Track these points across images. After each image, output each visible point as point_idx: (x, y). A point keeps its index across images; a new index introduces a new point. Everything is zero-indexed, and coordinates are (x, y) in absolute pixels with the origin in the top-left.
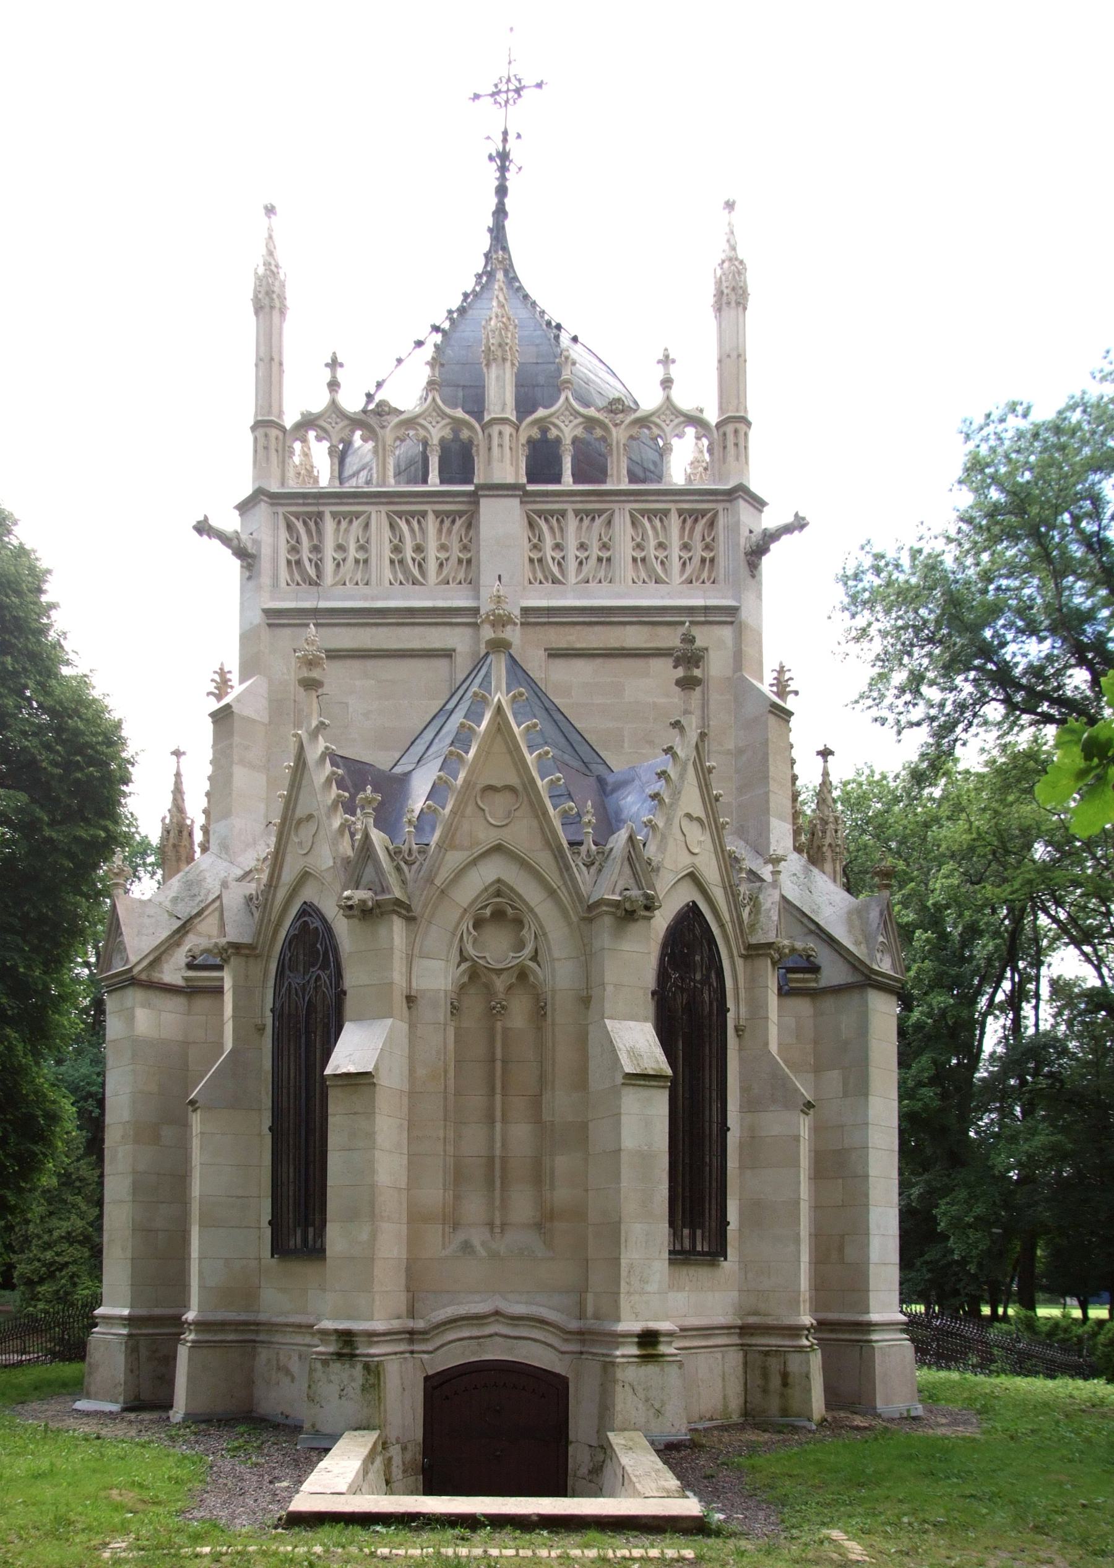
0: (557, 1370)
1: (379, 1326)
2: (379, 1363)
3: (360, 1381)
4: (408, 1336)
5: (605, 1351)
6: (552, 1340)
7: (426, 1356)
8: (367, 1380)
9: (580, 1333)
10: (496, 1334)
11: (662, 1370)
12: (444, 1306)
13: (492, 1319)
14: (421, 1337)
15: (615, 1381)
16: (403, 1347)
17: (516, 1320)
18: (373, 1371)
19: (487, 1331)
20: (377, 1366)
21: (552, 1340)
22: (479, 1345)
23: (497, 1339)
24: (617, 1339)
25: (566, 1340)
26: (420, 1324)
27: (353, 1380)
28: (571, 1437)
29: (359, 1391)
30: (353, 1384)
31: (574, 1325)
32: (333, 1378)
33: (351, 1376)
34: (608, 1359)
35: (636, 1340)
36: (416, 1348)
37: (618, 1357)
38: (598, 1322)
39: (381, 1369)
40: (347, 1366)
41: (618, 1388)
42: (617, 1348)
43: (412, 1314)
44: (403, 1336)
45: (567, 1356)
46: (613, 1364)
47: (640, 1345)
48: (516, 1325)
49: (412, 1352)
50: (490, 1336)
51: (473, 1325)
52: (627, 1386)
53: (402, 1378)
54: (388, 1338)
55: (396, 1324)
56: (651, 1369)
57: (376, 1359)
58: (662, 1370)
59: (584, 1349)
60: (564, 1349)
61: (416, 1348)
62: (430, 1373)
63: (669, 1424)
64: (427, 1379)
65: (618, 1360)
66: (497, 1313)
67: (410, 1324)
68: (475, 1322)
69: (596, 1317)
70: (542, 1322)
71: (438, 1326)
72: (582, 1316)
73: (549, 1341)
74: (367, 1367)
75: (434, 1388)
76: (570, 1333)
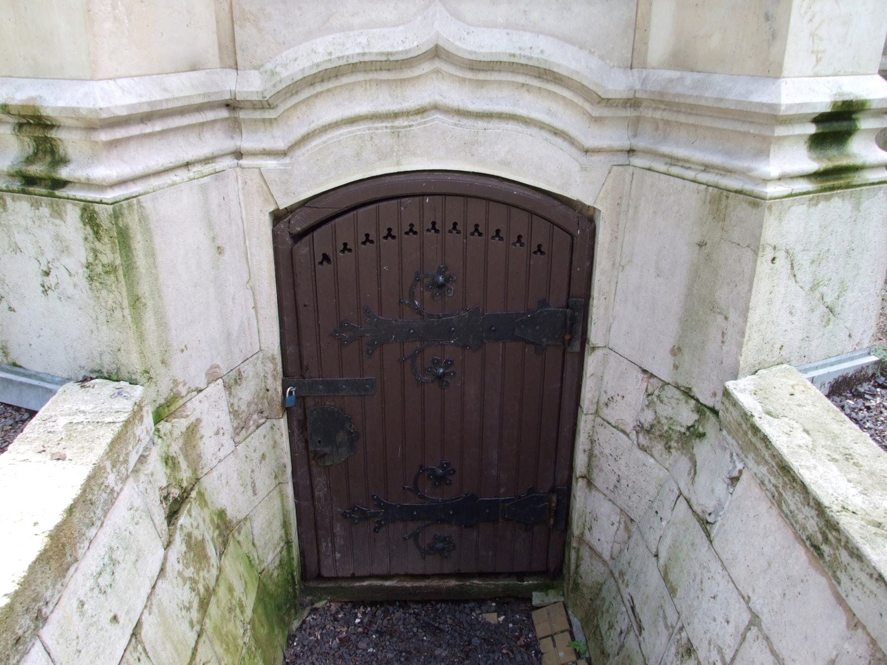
0: (572, 193)
1: (115, 96)
2: (117, 210)
3: (81, 253)
4: (224, 113)
5: (717, 159)
6: (566, 119)
7: (271, 164)
8: (95, 252)
9: (632, 103)
10: (436, 108)
11: (857, 207)
12: (310, 35)
13: (426, 67)
14: (258, 115)
15: (754, 246)
16: (214, 142)
17: (480, 68)
18: (112, 230)
19: (414, 98)
20: (116, 216)
21: (566, 119)
22: (396, 133)
23: (438, 116)
24: (760, 125)
25: (597, 120)
26: (250, 85)
27: (65, 250)
28: (596, 334)
29: (84, 283)
30: (66, 260)
31: (618, 84)
32: (21, 239)
33: (58, 237)
34: (733, 183)
35: (812, 129)
36: (247, 143)
37: (766, 181)
38: (690, 78)
39: (131, 220)
40: (45, 211)
41: (763, 266)
42: (763, 153)
43: (231, 57)
44: (210, 116)
45: (596, 158)
46: (756, 201)
47: (818, 142)
48: (481, 84)
49: (238, 154)
50: (421, 111)
51: (379, 83)
52: (781, 255)
53: (210, 225)
54: (158, 126)
55: (182, 87)
56: (837, 206)
57: (110, 195)
58: (857, 207)
59: (640, 143)
60: (590, 142)
61: (247, 143)
62: (284, 203)
63: (843, 335)
64: (278, 217)
65: (772, 190)
66: (437, 53)
67: (230, 84)
68: (384, 75)
69: (680, 60)
70: (546, 74)
71: (294, 88)
72: (635, 61)
73: (558, 124)
74: (89, 217)
75: (297, 237)
76: (607, 102)
